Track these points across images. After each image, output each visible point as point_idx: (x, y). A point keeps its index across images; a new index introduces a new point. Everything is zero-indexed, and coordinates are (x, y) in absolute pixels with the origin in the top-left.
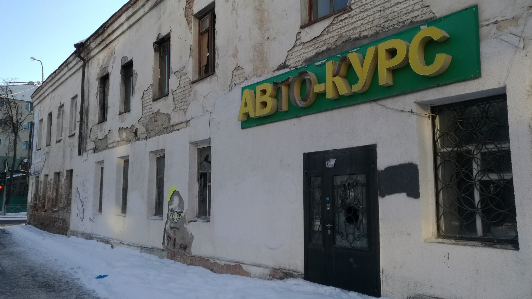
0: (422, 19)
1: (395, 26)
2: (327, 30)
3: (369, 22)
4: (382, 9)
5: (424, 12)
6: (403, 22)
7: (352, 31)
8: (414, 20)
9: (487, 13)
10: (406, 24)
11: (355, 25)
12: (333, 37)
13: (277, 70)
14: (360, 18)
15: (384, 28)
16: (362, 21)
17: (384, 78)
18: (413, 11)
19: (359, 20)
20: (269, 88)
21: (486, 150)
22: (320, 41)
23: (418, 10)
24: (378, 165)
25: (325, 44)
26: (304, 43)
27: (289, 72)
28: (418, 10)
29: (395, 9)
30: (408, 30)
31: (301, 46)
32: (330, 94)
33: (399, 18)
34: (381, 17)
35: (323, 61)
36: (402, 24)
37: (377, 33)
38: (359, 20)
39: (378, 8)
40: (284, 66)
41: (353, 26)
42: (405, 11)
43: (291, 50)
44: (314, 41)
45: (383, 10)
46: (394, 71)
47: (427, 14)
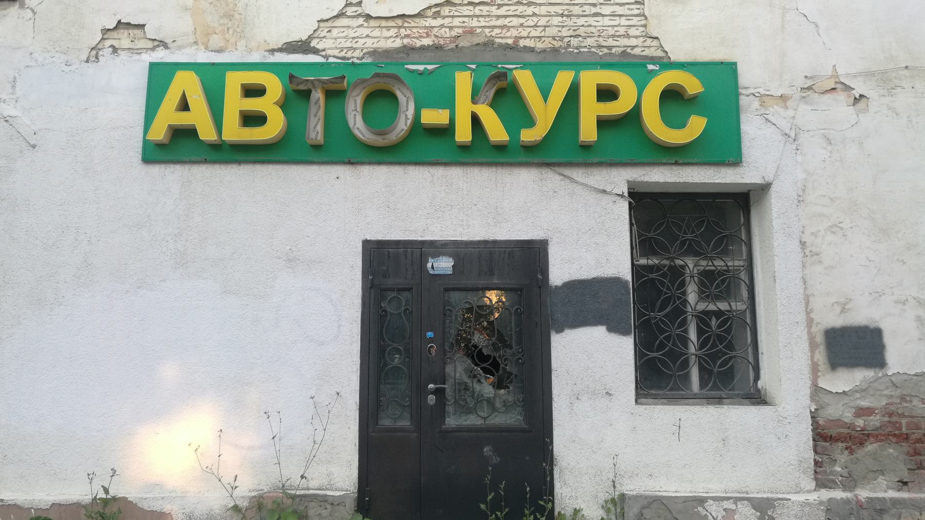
0: (644, 53)
1: (593, 50)
2: (434, 10)
3: (536, 26)
4: (566, 13)
5: (646, 44)
6: (610, 48)
7: (497, 31)
8: (629, 50)
9: (748, 77)
10: (613, 51)
11: (506, 22)
12: (451, 28)
13: (280, 50)
14: (517, 13)
15: (569, 46)
16: (522, 20)
17: (588, 131)
18: (628, 36)
19: (513, 16)
20: (275, 87)
21: (713, 268)
22: (413, 24)
23: (636, 37)
24: (551, 276)
25: (428, 35)
26: (368, 17)
27: (322, 64)
28: (636, 37)
29: (591, 20)
30: (637, 66)
31: (361, 21)
32: (464, 133)
33: (601, 39)
34: (563, 27)
35: (430, 67)
36: (606, 51)
37: (555, 50)
38: (513, 16)
39: (559, 9)
40: (303, 47)
41: (500, 22)
42: (611, 31)
43: (327, 20)
44: (399, 22)
45: (567, 16)
46: (603, 123)
47: (653, 49)
